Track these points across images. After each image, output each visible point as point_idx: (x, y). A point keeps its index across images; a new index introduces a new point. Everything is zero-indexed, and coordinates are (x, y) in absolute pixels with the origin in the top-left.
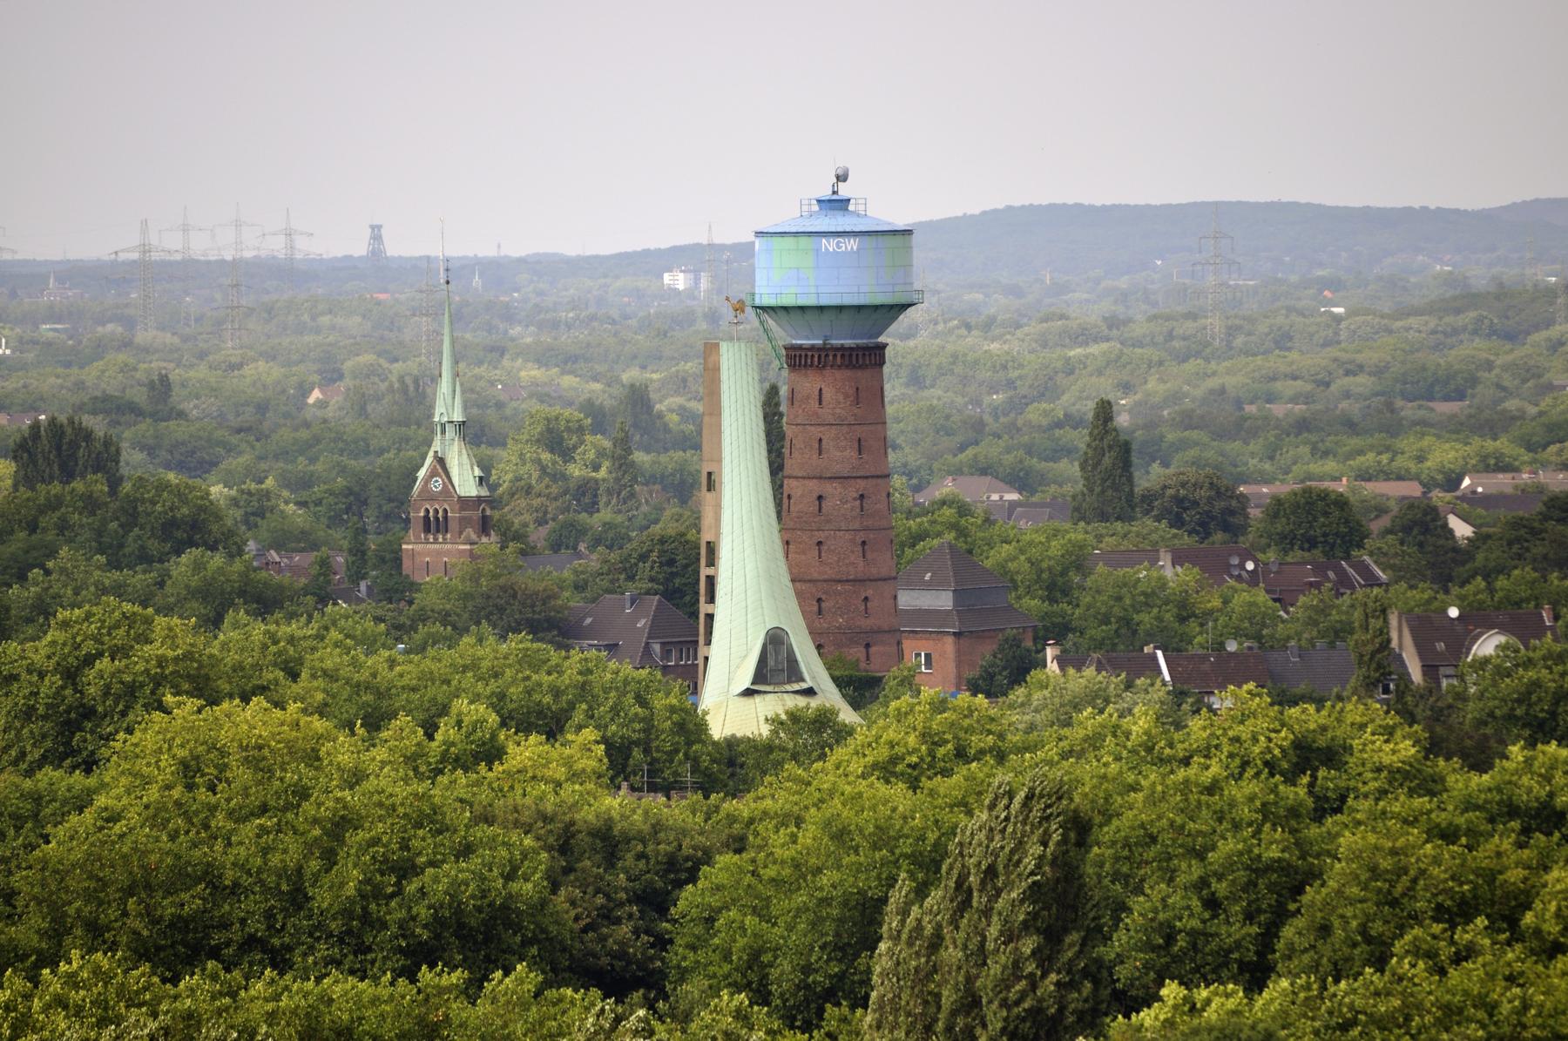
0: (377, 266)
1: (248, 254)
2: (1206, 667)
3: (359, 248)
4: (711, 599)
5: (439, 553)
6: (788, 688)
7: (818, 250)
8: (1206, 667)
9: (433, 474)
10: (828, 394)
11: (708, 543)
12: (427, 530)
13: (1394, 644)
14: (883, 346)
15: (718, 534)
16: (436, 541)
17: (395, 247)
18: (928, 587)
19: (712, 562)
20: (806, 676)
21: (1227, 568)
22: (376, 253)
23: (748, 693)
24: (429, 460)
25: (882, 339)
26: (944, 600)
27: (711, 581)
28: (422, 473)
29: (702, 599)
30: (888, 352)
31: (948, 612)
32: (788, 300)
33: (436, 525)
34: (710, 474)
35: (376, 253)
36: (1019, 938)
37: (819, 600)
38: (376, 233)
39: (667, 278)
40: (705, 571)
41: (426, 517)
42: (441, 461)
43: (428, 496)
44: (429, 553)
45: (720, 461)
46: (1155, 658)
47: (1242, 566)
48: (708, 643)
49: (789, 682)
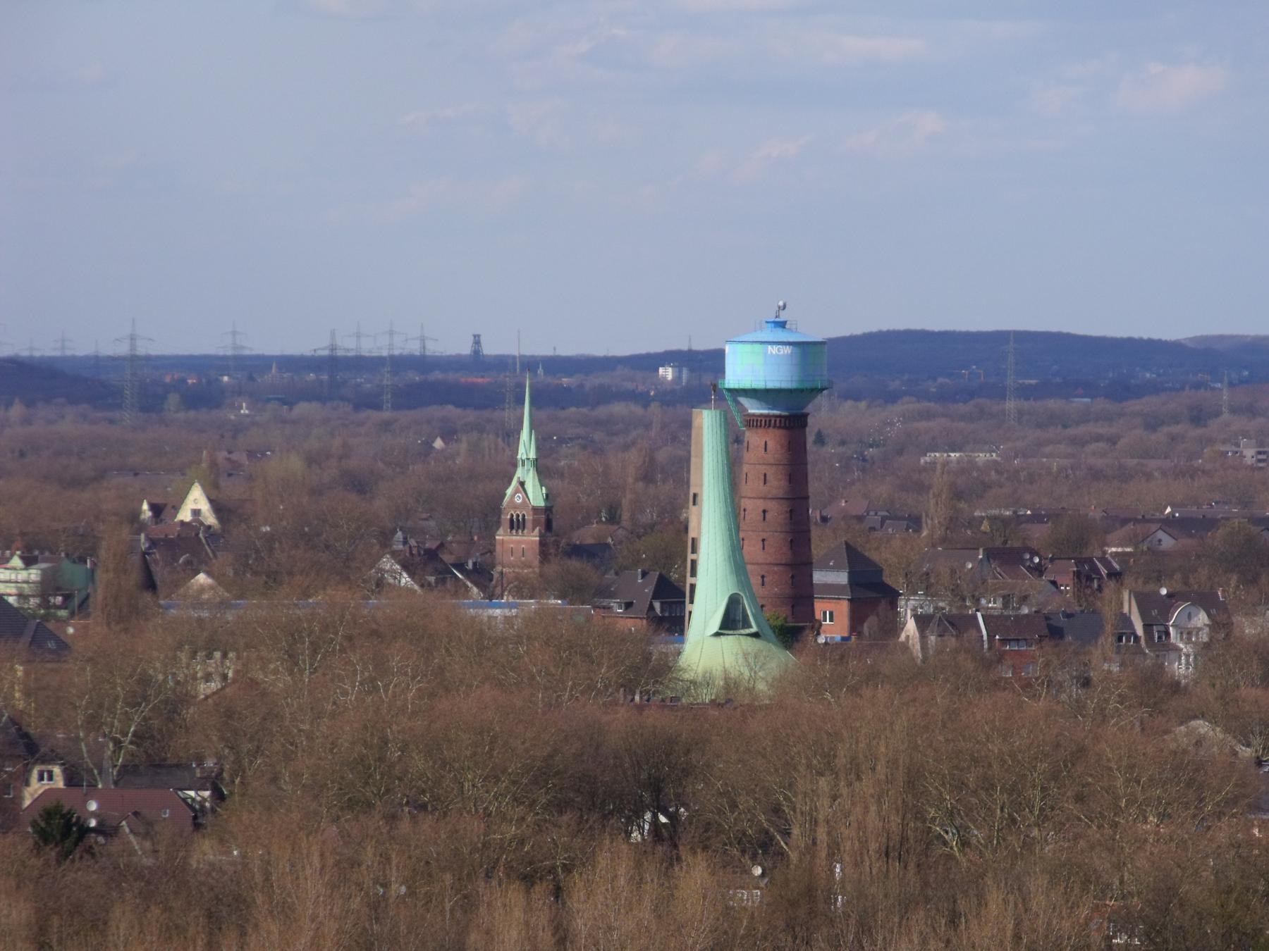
0: (31, 358)
1: (397, 352)
2: (1009, 623)
3: (465, 349)
4: (694, 574)
5: (519, 542)
6: (743, 632)
7: (766, 354)
8: (1009, 623)
9: (516, 492)
10: (771, 445)
11: (693, 539)
12: (512, 528)
13: (1126, 610)
14: (807, 415)
15: (699, 533)
16: (517, 534)
17: (489, 349)
18: (834, 568)
19: (694, 551)
20: (753, 624)
21: (1022, 561)
22: (477, 352)
23: (717, 634)
24: (514, 482)
25: (805, 411)
26: (842, 578)
27: (694, 563)
28: (509, 491)
29: (688, 574)
30: (810, 420)
31: (844, 586)
32: (760, 385)
33: (517, 525)
34: (695, 495)
35: (477, 352)
36: (445, 564)
37: (763, 577)
38: (477, 340)
39: (661, 370)
40: (690, 556)
41: (511, 520)
42: (522, 484)
43: (516, 507)
44: (512, 542)
45: (701, 485)
46: (975, 617)
47: (1031, 559)
48: (692, 602)
49: (743, 628)
